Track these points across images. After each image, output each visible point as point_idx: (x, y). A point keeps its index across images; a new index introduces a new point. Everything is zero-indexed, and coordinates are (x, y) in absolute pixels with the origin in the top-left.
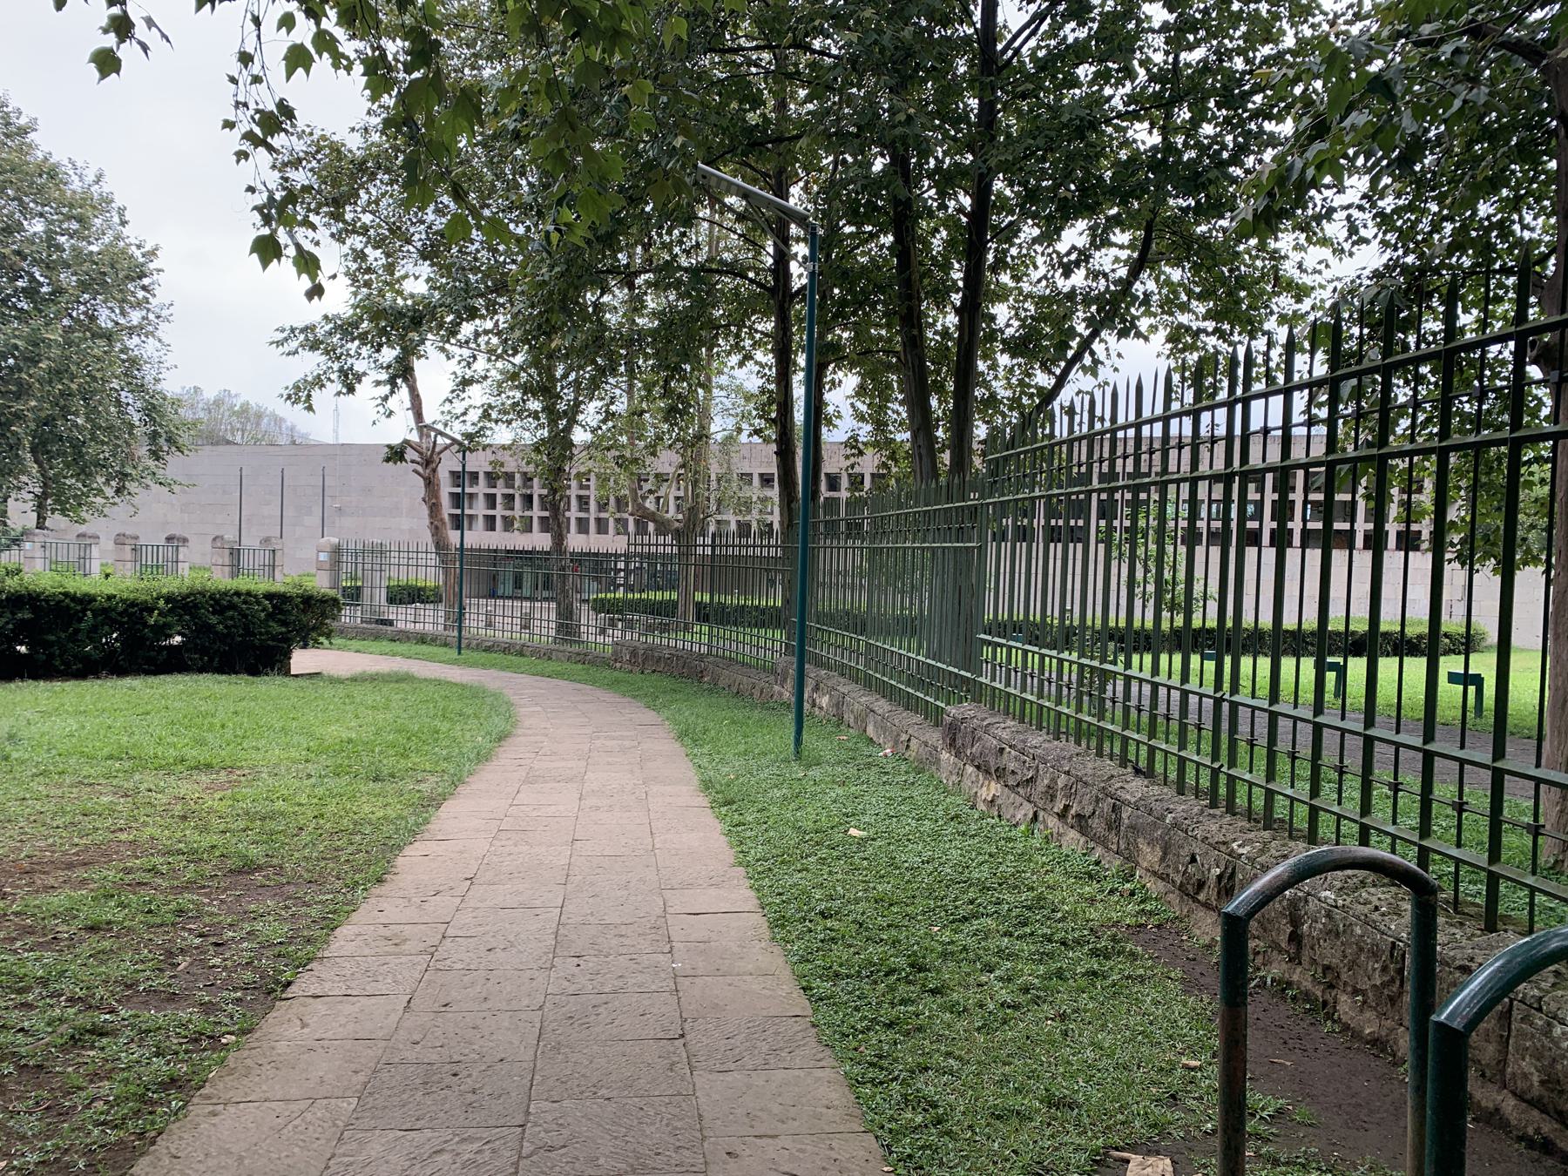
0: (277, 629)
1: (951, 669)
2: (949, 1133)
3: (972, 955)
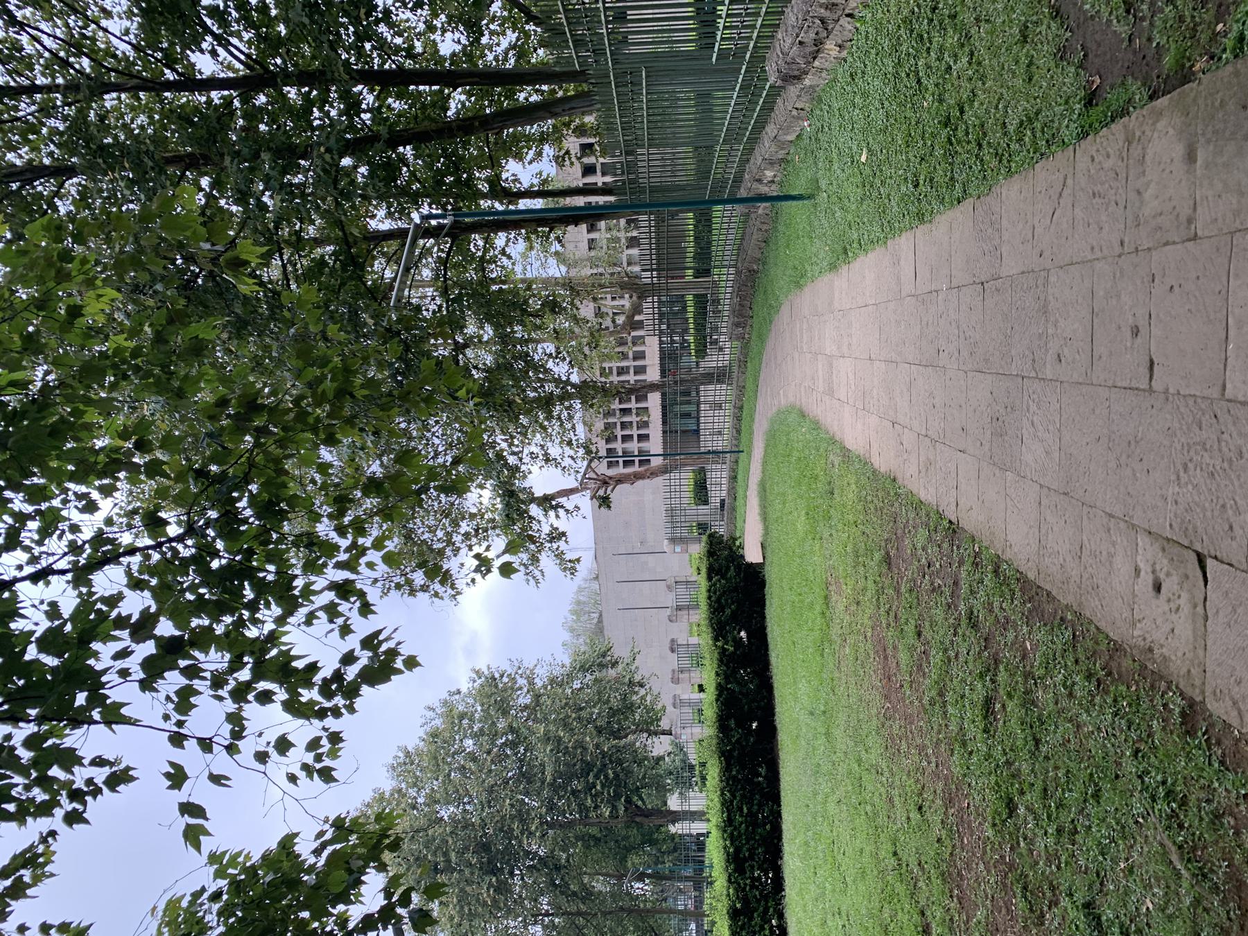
0: (732, 573)
1: (740, 80)
2: (1037, 114)
3: (941, 81)
